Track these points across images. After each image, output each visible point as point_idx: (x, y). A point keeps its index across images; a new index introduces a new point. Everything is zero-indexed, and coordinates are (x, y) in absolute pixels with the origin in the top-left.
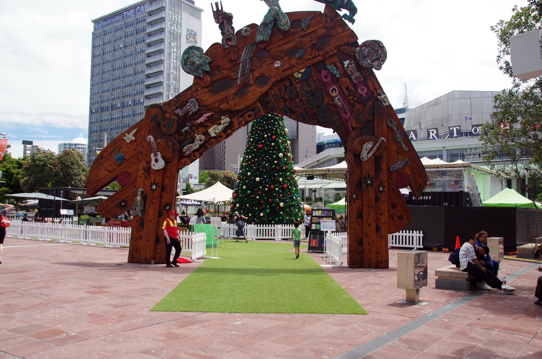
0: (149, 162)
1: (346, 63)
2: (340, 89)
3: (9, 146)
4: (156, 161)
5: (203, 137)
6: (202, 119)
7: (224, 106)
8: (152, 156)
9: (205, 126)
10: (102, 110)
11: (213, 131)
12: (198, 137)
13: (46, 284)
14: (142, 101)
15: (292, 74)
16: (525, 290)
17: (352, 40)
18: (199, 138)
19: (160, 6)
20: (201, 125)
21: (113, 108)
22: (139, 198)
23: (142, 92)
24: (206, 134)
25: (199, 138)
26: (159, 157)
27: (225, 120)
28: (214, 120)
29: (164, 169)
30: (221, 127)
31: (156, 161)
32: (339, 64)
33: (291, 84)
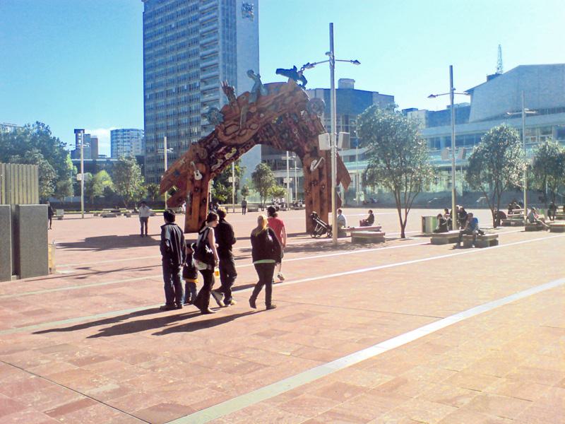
0: (193, 176)
1: (302, 112)
2: (298, 128)
3: (384, 234)
4: (197, 175)
5: (222, 161)
6: (221, 150)
7: (233, 142)
8: (195, 172)
9: (223, 154)
10: (157, 96)
11: (228, 156)
12: (219, 161)
13: (234, 138)
14: (198, 85)
15: (271, 121)
16: (314, 248)
17: (305, 99)
18: (220, 161)
19: (213, 74)
20: (221, 153)
21: (179, 125)
22: (188, 196)
23: (198, 76)
24: (224, 158)
25: (220, 161)
26: (199, 173)
27: (234, 150)
28: (228, 151)
29: (202, 180)
30: (231, 154)
31: (197, 175)
32: (297, 114)
33: (271, 127)
